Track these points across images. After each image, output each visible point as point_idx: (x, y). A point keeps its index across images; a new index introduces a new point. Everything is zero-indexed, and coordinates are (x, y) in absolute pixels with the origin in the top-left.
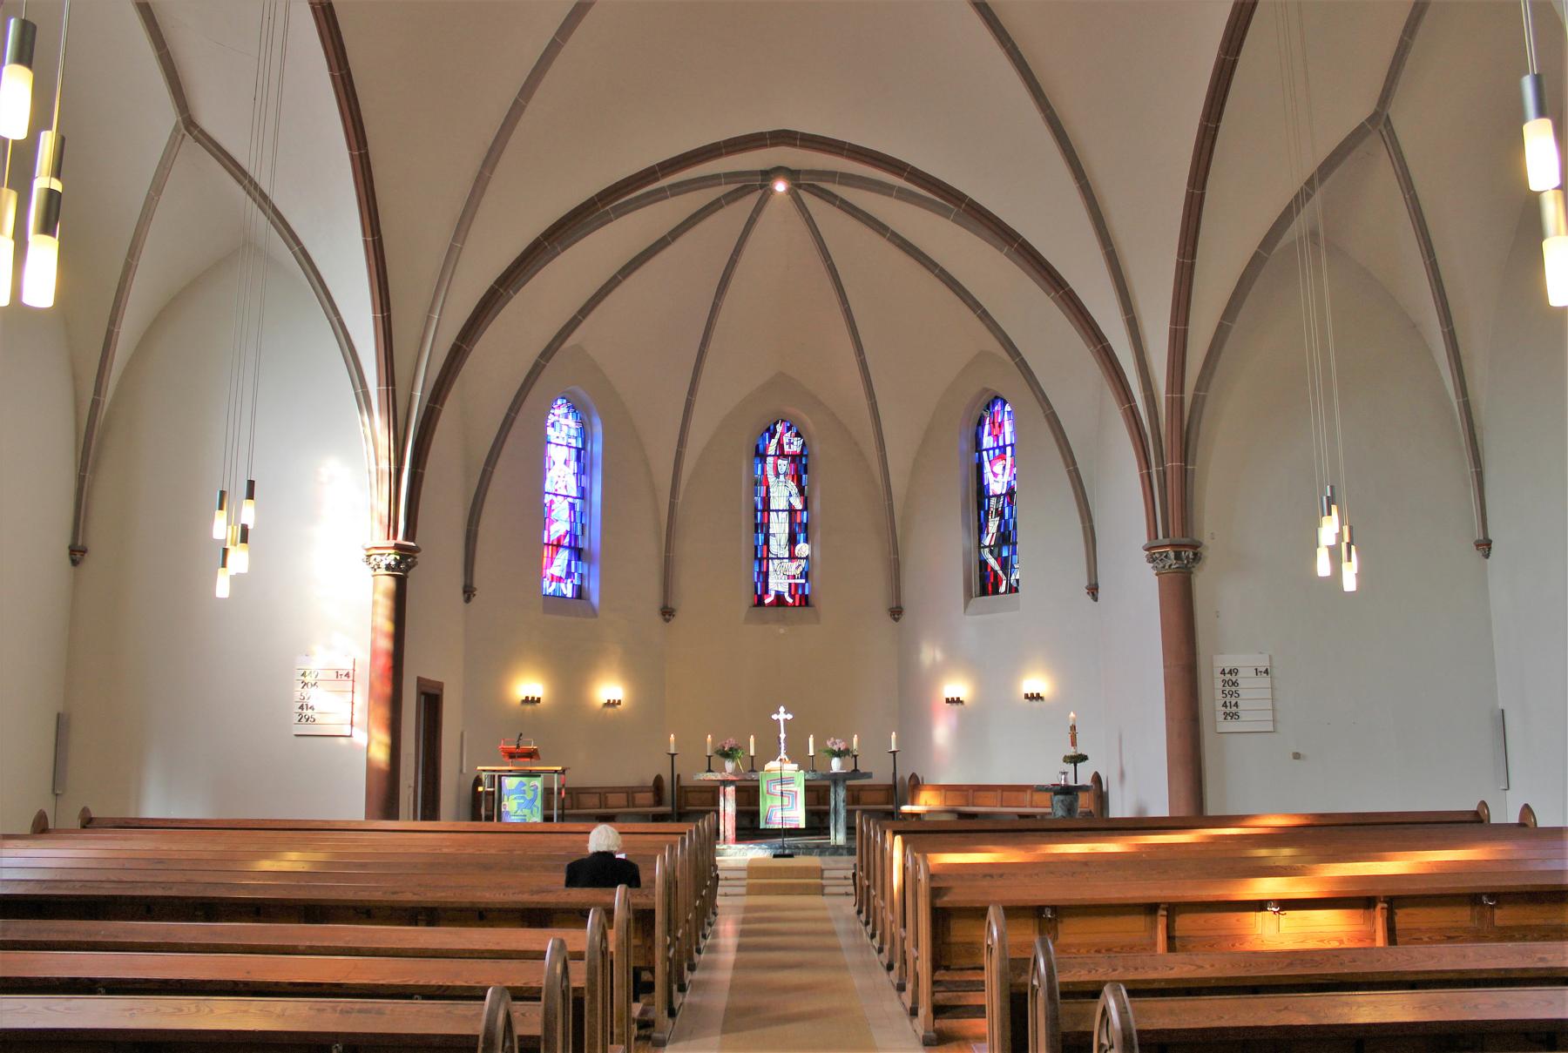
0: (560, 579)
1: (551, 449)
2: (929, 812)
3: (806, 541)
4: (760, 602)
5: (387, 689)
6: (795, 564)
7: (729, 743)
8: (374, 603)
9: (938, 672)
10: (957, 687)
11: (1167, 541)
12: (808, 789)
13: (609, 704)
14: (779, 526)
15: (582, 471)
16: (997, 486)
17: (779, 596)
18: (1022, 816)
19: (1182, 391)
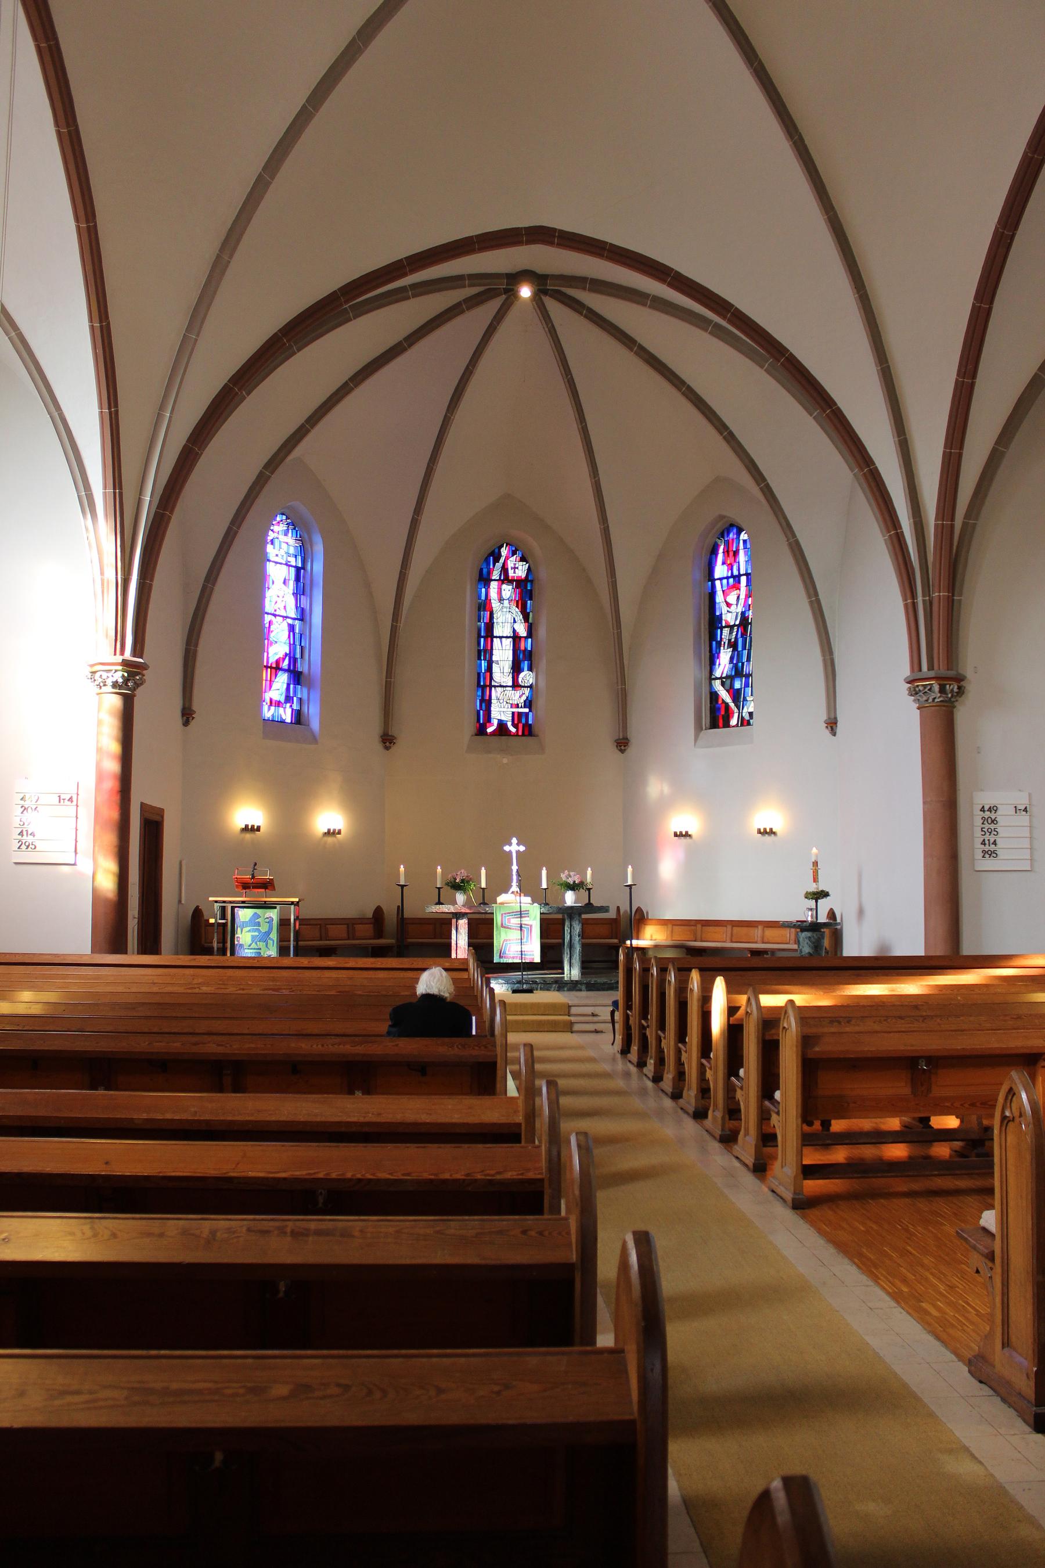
0: (278, 704)
1: (270, 567)
2: (656, 946)
3: (530, 669)
4: (481, 730)
5: (115, 815)
6: (518, 693)
7: (460, 875)
8: (100, 723)
9: (666, 805)
10: (685, 818)
11: (932, 674)
12: (543, 922)
13: (329, 833)
14: (503, 653)
15: (300, 592)
16: (730, 617)
17: (502, 725)
18: (756, 953)
19: (953, 519)
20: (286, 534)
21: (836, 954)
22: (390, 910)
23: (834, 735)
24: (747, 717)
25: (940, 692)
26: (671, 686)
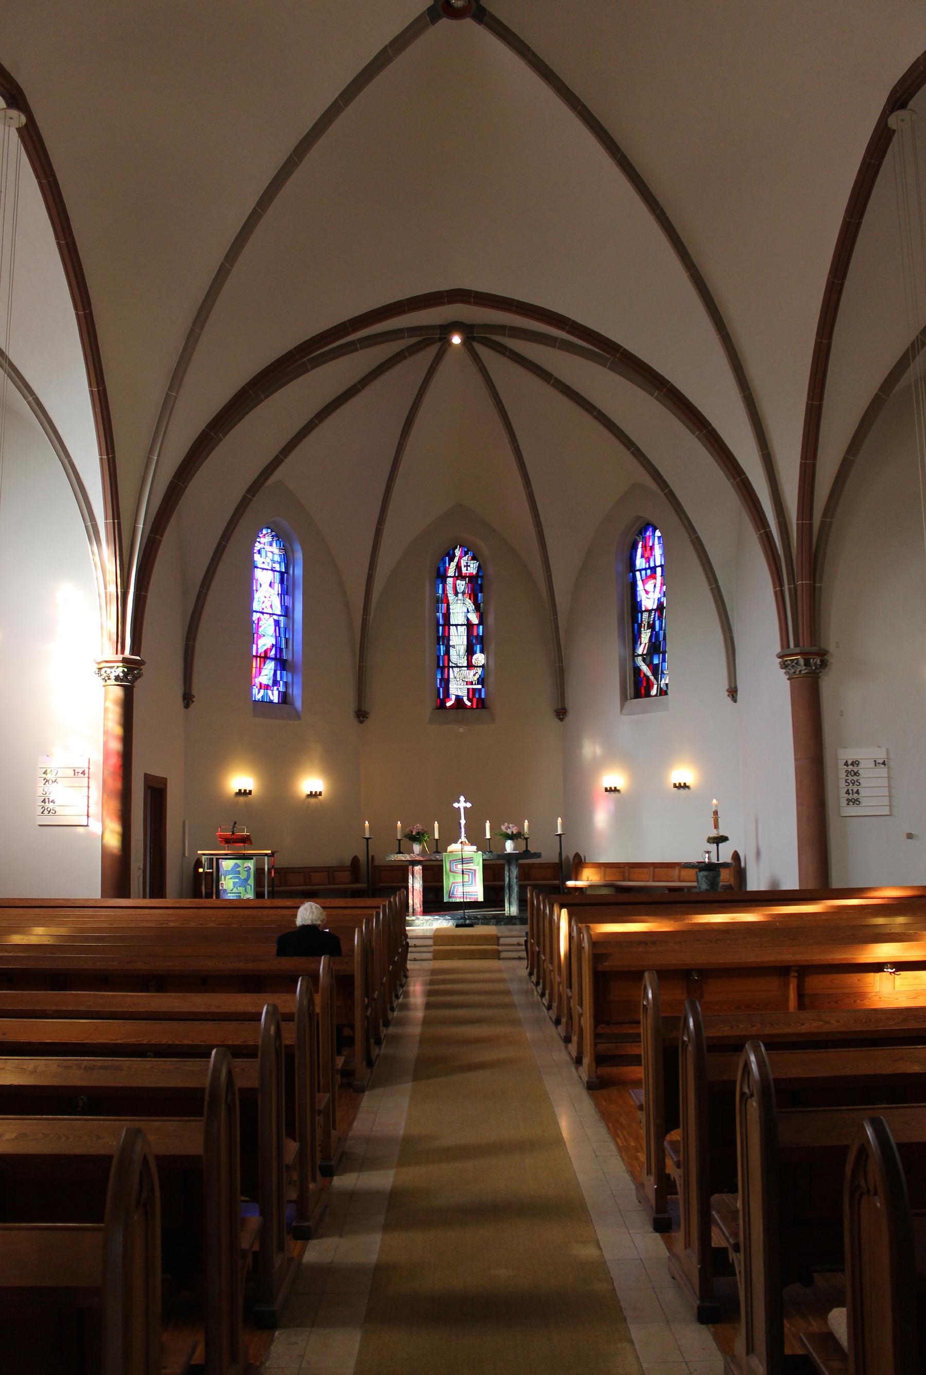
0: (267, 687)
2: (590, 886)
3: (482, 652)
4: (442, 705)
5: (118, 785)
6: (472, 672)
7: (418, 827)
8: (106, 710)
9: (598, 765)
11: (797, 650)
12: (485, 867)
13: (311, 795)
14: (458, 639)
15: (286, 591)
17: (459, 699)
19: (811, 518)
20: (271, 545)
21: (741, 889)
22: (362, 858)
23: (735, 701)
24: (665, 688)
25: (805, 665)
26: (601, 662)
